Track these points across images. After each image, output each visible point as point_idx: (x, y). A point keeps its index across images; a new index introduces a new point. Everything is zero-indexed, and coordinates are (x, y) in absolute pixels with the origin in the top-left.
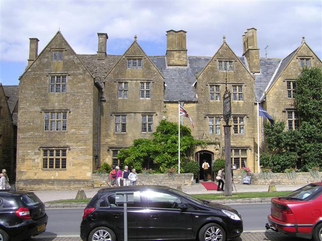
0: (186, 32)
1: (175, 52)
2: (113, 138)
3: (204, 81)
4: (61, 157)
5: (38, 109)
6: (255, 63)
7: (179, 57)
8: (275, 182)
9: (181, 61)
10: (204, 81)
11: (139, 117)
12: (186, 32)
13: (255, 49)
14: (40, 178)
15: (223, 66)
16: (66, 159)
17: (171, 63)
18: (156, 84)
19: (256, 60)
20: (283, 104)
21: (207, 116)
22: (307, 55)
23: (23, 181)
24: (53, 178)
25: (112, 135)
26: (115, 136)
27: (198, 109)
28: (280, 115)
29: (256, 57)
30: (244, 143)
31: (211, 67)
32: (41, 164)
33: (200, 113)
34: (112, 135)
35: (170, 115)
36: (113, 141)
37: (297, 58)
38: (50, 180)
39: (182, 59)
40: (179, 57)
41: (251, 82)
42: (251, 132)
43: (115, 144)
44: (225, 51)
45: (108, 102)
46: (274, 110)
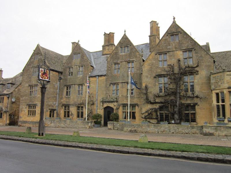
0: (114, 33)
1: (106, 47)
2: (64, 100)
3: (111, 62)
4: (220, 103)
5: (27, 85)
6: (153, 46)
7: (108, 49)
8: (133, 130)
9: (109, 51)
10: (111, 62)
11: (77, 87)
12: (114, 33)
13: (153, 36)
14: (26, 121)
15: (123, 51)
16: (65, 110)
17: (104, 54)
18: (85, 67)
19: (153, 43)
20: (155, 71)
21: (111, 84)
22: (175, 31)
23: (21, 121)
24: (30, 120)
25: (64, 98)
26: (65, 98)
27: (106, 80)
28: (152, 80)
29: (154, 41)
30: (134, 102)
31: (115, 52)
32: (27, 113)
33: (107, 82)
34: (64, 98)
35: (92, 85)
36: (64, 101)
37: (167, 36)
38: (29, 122)
39: (110, 50)
40: (108, 49)
41: (139, 59)
43: (65, 103)
44: (125, 40)
45: (64, 79)
46: (148, 76)
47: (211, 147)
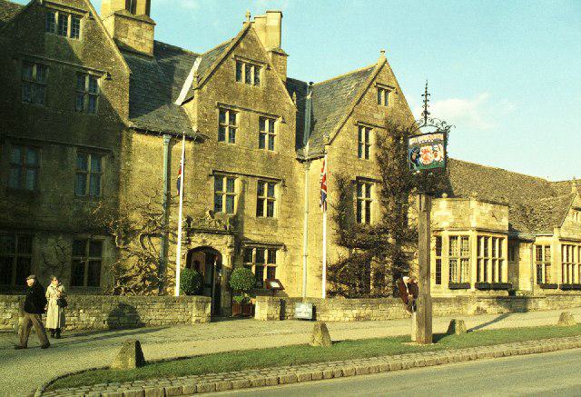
9: (142, 44)
39: (143, 41)
42: (287, 215)
47: (340, 345)
